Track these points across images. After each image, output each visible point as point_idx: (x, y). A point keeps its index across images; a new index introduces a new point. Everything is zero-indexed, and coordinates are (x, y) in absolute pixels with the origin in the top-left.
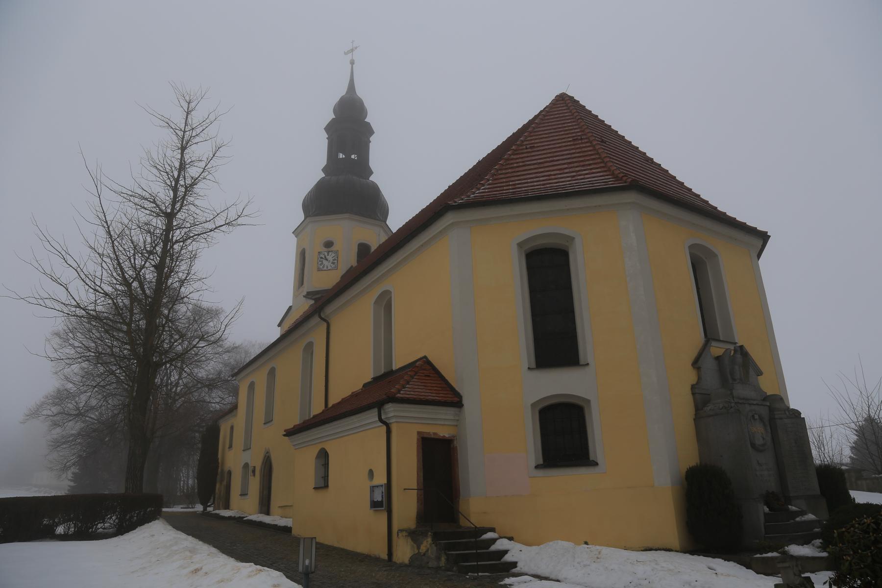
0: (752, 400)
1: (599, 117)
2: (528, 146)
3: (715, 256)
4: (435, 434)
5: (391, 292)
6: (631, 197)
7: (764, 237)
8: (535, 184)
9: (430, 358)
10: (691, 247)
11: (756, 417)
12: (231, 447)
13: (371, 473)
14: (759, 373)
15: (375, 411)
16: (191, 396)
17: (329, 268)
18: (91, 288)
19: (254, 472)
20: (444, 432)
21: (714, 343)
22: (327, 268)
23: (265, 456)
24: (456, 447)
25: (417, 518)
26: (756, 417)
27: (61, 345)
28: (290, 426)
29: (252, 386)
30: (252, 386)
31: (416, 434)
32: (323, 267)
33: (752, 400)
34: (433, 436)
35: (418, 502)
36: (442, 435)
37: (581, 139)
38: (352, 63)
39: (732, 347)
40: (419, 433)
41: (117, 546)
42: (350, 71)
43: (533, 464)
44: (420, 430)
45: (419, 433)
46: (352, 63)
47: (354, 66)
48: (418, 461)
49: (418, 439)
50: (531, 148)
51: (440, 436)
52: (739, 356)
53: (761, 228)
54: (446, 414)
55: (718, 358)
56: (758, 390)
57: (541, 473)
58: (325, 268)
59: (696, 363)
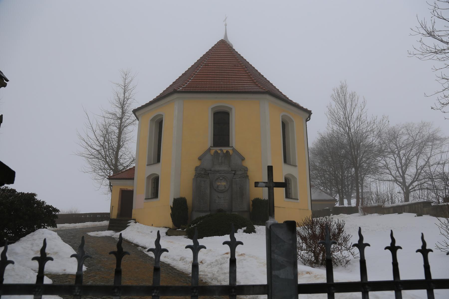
0: (221, 171)
1: (241, 55)
3: (293, 121)
4: (126, 189)
6: (268, 97)
7: (310, 113)
8: (238, 89)
9: (197, 166)
10: (282, 116)
16: (337, 198)
18: (393, 160)
33: (221, 171)
34: (126, 190)
35: (118, 211)
36: (129, 189)
37: (238, 66)
38: (226, 25)
41: (179, 244)
42: (225, 28)
45: (120, 189)
46: (226, 25)
47: (227, 27)
48: (119, 198)
49: (120, 191)
53: (309, 109)
54: (129, 182)
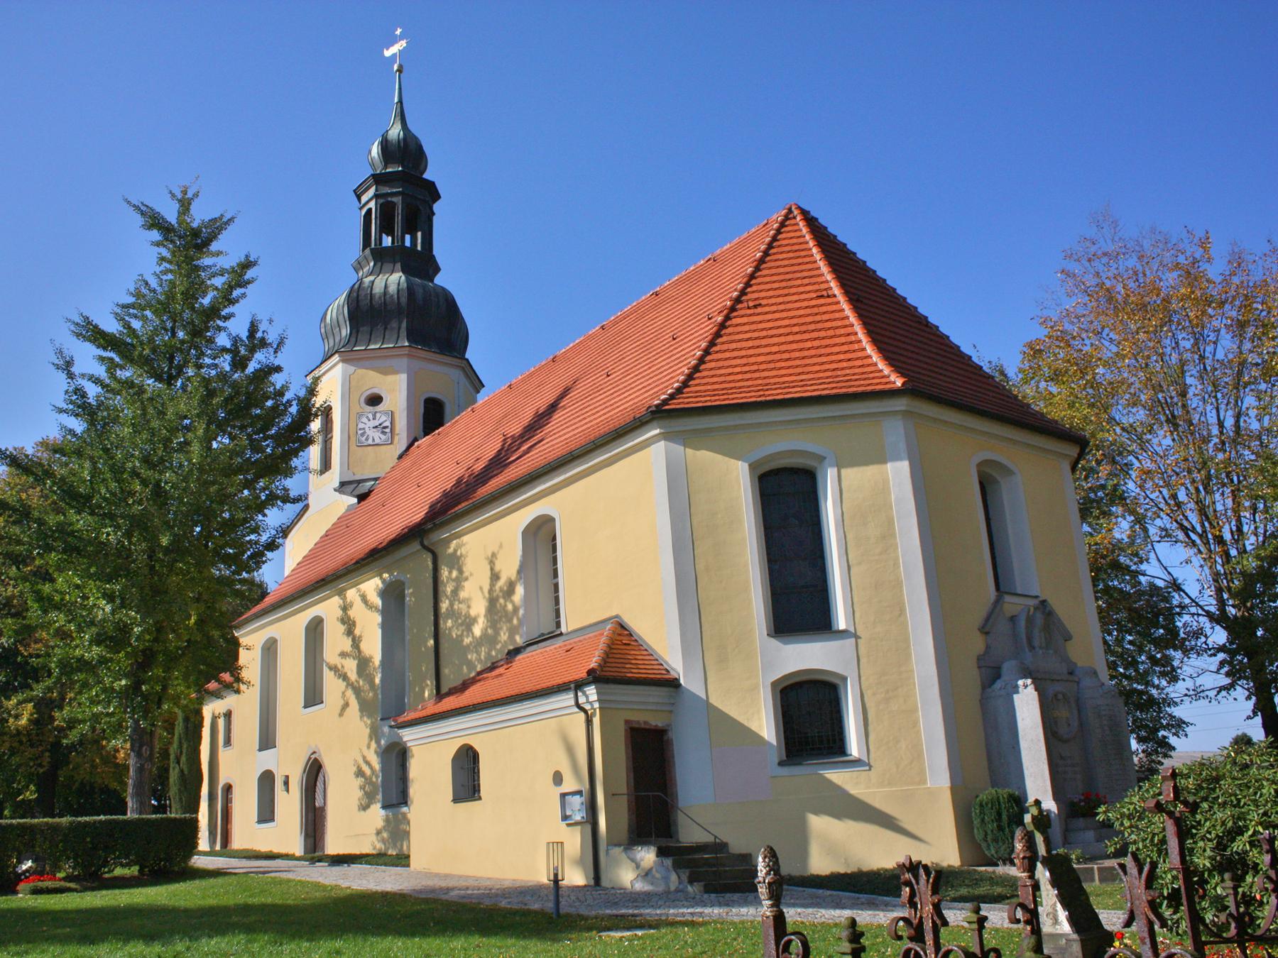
2: (751, 304)
4: (645, 723)
5: (553, 520)
11: (1060, 696)
12: (228, 742)
13: (558, 778)
14: (1068, 637)
15: (571, 695)
17: (377, 441)
19: (286, 783)
20: (656, 721)
21: (1008, 598)
22: (373, 440)
23: (310, 758)
24: (672, 740)
25: (629, 831)
26: (1060, 696)
27: (1032, 740)
28: (339, 711)
29: (270, 649)
30: (270, 649)
31: (622, 723)
32: (367, 439)
34: (643, 726)
36: (654, 724)
39: (1032, 602)
40: (627, 722)
43: (776, 761)
44: (628, 718)
45: (627, 722)
49: (626, 730)
50: (755, 307)
51: (651, 725)
52: (1039, 615)
55: (1013, 619)
56: (1066, 659)
57: (786, 771)
58: (370, 442)
59: (985, 630)
